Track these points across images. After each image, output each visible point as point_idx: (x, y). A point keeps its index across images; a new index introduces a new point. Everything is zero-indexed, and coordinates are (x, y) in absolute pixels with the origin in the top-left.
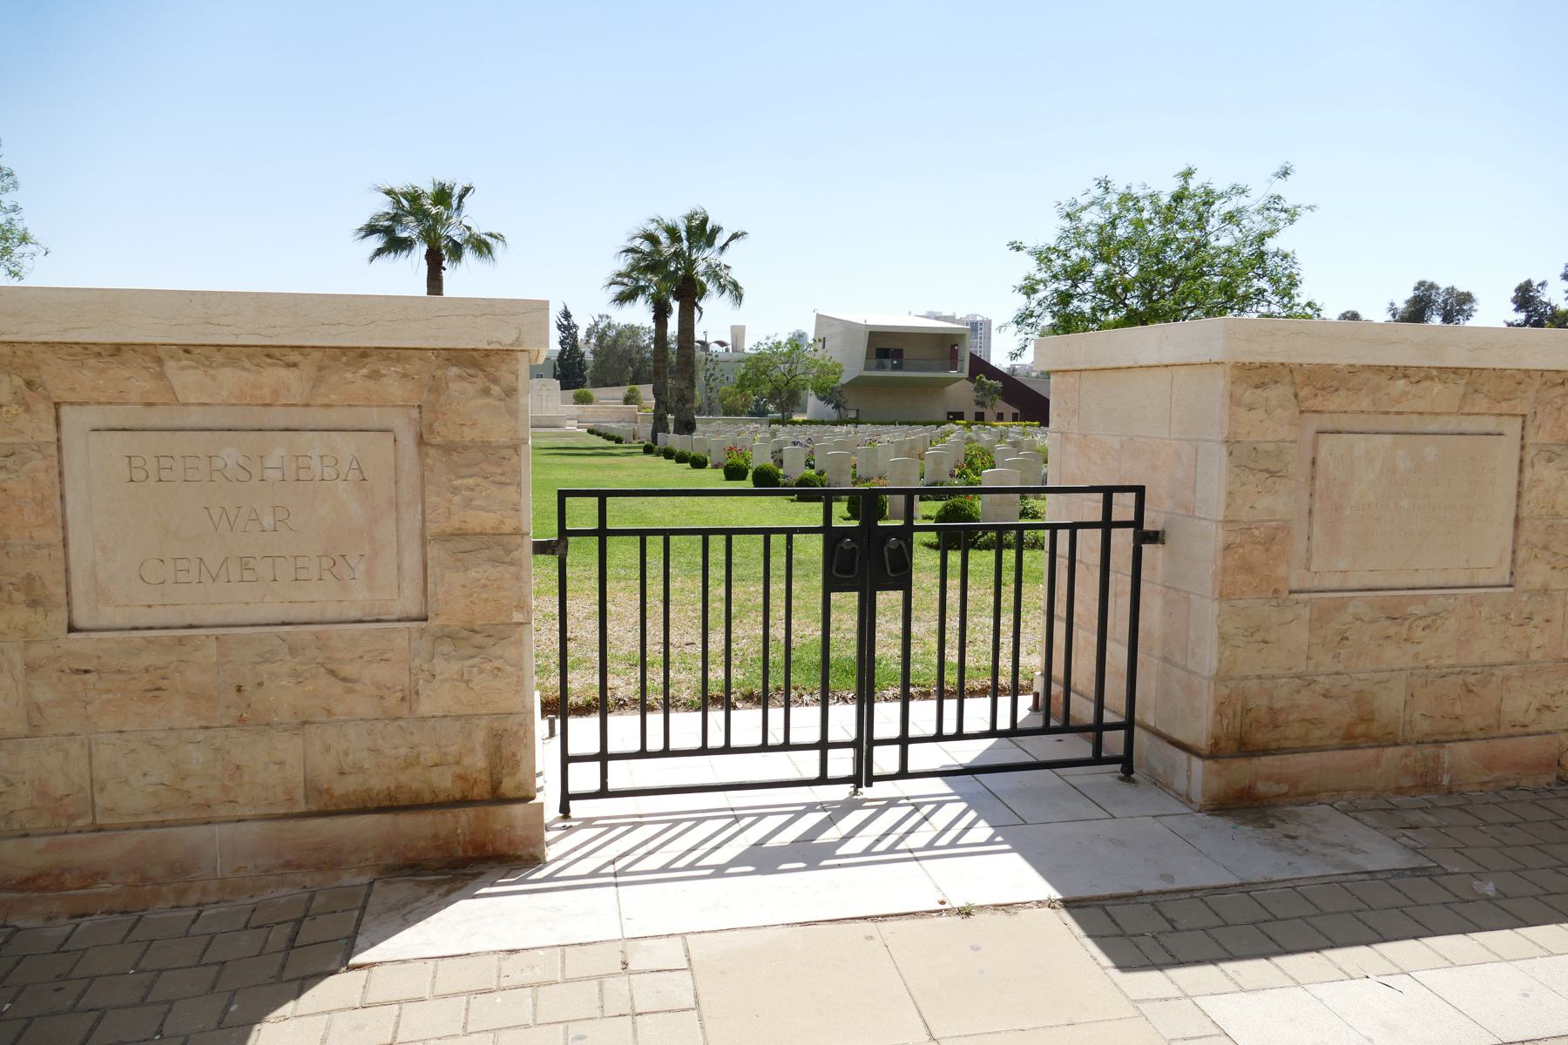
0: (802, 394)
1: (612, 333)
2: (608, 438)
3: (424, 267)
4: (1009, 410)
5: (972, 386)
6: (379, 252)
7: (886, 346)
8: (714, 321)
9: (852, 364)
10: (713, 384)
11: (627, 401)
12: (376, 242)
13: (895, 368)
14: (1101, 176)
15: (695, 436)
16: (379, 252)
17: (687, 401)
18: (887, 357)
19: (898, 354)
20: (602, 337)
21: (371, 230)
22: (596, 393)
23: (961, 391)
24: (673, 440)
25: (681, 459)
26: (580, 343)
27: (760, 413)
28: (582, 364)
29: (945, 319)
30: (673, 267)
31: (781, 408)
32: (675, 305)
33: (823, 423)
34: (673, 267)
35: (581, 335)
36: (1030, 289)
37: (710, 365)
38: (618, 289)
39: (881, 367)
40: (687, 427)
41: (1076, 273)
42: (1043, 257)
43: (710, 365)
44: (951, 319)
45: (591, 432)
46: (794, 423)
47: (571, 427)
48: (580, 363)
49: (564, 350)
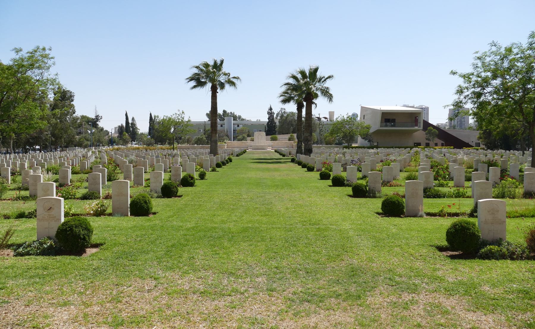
0: (356, 137)
1: (285, 115)
2: (281, 154)
3: (210, 93)
4: (440, 142)
5: (424, 133)
6: (195, 87)
7: (389, 118)
8: (321, 109)
9: (375, 125)
10: (322, 133)
11: (290, 140)
12: (193, 83)
13: (392, 126)
14: (491, 42)
15: (312, 155)
16: (195, 87)
17: (309, 141)
18: (389, 122)
19: (394, 121)
20: (282, 116)
21: (191, 79)
22: (279, 137)
23: (420, 134)
24: (302, 158)
25: (304, 166)
26: (275, 119)
27: (340, 144)
28: (275, 127)
29: (413, 107)
30: (304, 88)
31: (348, 142)
32: (305, 103)
33: (364, 147)
34: (304, 88)
35: (275, 116)
36: (460, 91)
37: (321, 126)
38: (282, 98)
39: (386, 126)
40: (309, 151)
41: (485, 83)
42: (467, 77)
43: (321, 126)
44: (413, 107)
45: (276, 151)
46: (353, 148)
47: (269, 149)
48: (274, 126)
49: (269, 121)
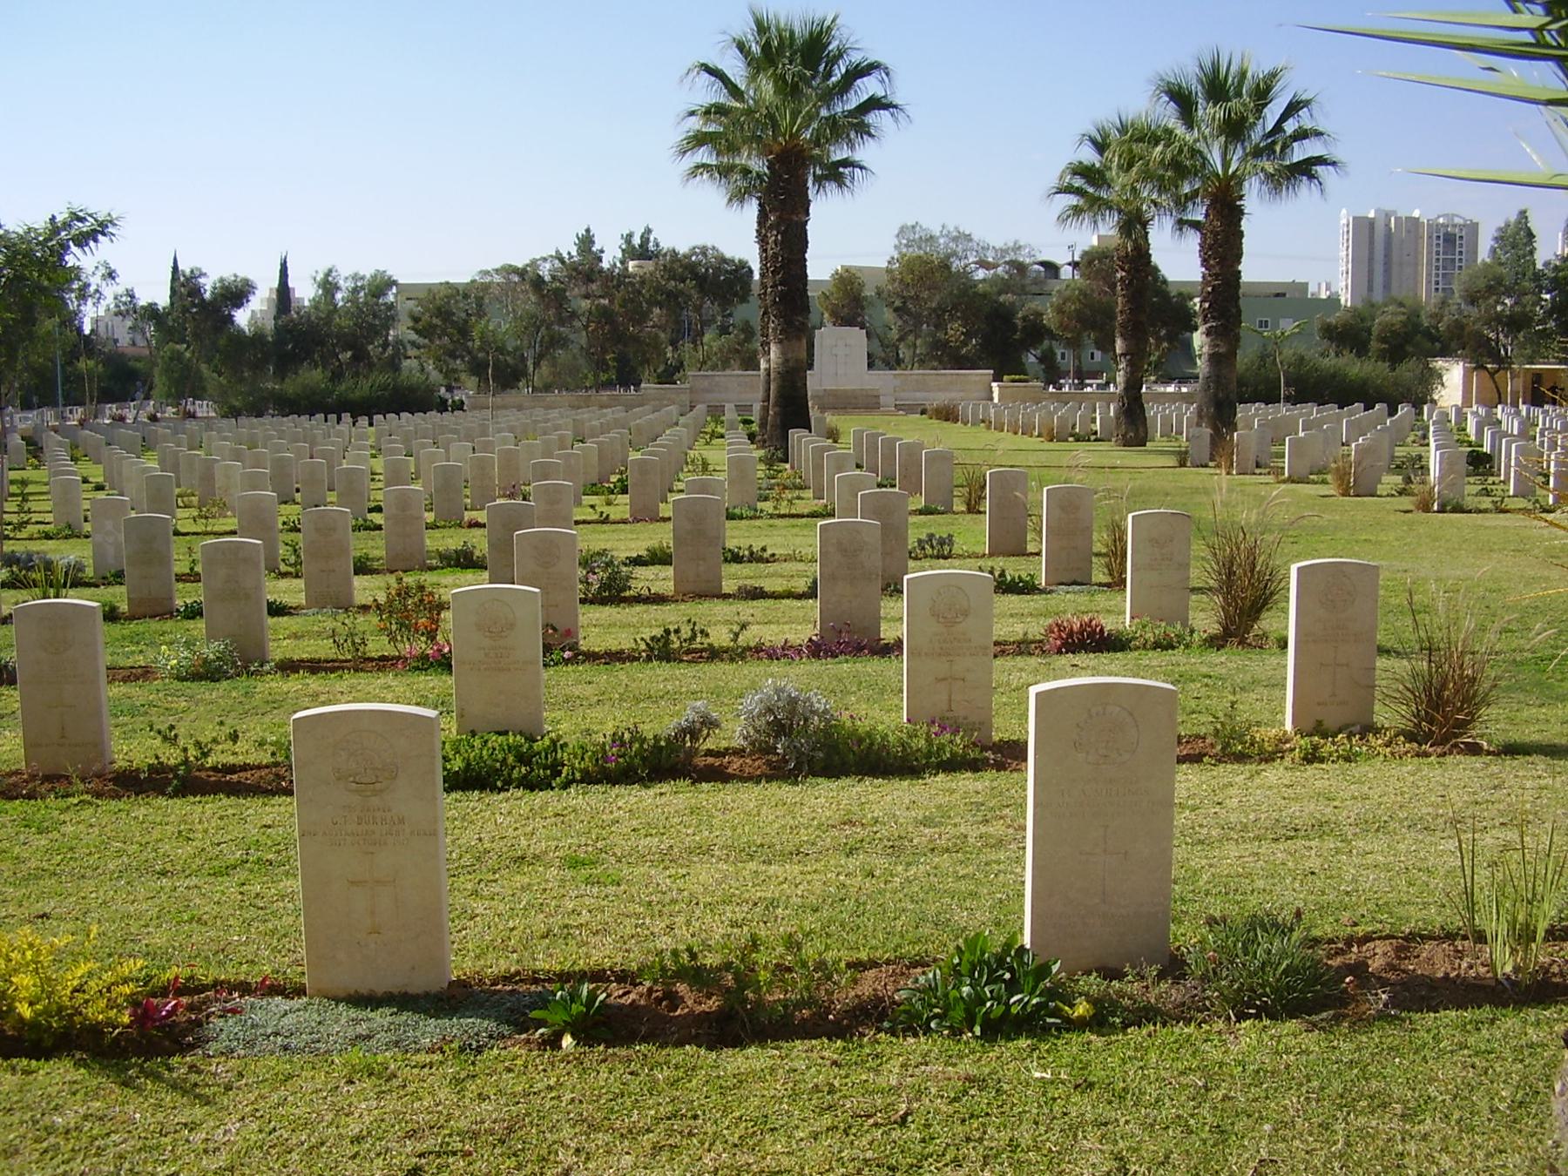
30: (1220, 137)
